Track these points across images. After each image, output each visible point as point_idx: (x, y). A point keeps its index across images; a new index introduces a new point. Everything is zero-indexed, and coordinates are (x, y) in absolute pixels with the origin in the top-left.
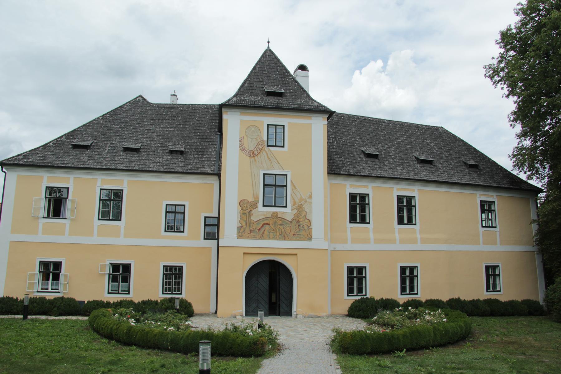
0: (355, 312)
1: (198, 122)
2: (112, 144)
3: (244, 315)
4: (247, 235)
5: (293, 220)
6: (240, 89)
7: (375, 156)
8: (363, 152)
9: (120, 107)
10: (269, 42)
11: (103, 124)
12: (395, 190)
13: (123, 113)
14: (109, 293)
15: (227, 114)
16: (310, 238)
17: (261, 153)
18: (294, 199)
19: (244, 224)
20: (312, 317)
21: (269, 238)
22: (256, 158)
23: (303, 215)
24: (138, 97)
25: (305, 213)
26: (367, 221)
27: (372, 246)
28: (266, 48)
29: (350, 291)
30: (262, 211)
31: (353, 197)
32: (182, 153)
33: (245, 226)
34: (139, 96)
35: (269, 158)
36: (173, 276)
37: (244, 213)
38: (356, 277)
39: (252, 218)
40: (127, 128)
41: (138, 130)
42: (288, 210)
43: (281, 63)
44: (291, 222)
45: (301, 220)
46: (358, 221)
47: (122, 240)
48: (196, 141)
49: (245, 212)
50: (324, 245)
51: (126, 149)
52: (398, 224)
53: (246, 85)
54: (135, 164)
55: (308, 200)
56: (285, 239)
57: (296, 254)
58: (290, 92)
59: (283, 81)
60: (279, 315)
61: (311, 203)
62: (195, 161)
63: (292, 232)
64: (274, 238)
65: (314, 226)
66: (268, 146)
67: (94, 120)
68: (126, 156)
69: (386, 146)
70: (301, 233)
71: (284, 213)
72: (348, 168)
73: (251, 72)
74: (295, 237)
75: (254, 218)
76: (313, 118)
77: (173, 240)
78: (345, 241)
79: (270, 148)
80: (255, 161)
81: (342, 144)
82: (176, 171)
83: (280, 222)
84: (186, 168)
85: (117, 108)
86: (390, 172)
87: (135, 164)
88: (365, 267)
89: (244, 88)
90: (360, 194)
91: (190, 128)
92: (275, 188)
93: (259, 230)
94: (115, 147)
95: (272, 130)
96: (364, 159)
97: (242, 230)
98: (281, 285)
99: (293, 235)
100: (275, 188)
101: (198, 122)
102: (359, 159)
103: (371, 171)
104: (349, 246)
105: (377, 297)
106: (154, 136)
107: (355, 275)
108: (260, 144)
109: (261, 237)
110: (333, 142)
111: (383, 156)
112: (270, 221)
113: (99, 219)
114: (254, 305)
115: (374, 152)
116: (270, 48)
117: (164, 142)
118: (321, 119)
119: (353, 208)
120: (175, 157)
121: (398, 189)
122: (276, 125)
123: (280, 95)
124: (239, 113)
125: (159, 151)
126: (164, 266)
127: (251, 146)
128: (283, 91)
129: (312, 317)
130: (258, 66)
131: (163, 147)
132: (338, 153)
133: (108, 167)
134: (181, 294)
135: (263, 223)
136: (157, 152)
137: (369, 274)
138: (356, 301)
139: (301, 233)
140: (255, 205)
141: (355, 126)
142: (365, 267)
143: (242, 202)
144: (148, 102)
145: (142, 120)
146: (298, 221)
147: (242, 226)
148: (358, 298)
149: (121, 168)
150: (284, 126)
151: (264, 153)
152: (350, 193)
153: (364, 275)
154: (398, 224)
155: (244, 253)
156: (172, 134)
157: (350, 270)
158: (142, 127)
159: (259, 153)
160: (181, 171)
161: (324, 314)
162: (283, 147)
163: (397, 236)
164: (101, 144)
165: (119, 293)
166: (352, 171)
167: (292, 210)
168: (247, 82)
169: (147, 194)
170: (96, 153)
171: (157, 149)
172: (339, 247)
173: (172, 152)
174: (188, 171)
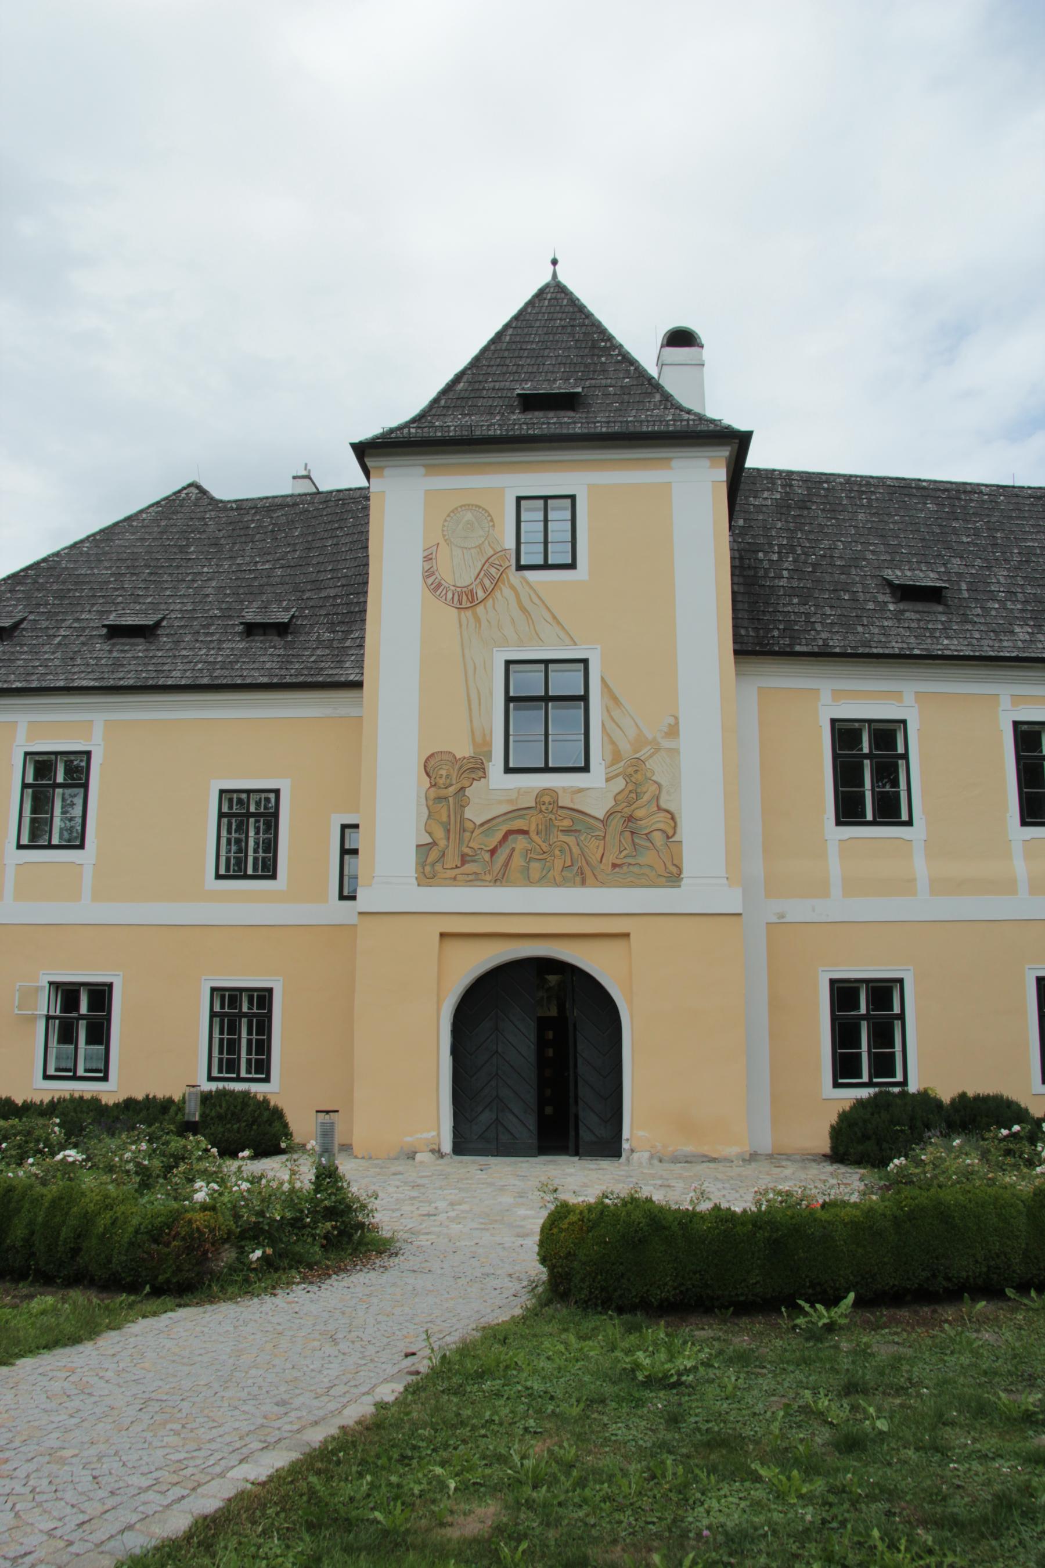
0: (856, 1141)
1: (348, 539)
2: (77, 620)
3: (447, 1146)
4: (452, 873)
5: (610, 814)
6: (435, 401)
7: (932, 595)
8: (889, 583)
9: (129, 519)
10: (554, 262)
11: (66, 568)
12: (1005, 702)
13: (133, 533)
14: (46, 1077)
15: (382, 476)
16: (674, 877)
17: (497, 594)
18: (613, 742)
19: (440, 834)
20: (688, 1160)
21: (529, 881)
22: (480, 609)
23: (646, 797)
24: (184, 488)
25: (654, 788)
26: (905, 817)
27: (923, 906)
28: (547, 278)
29: (845, 1068)
30: (500, 789)
31: (845, 734)
32: (281, 629)
33: (442, 843)
34: (190, 485)
35: (523, 609)
36: (243, 1020)
37: (439, 799)
38: (865, 1018)
39: (468, 813)
40: (133, 574)
41: (165, 577)
42: (596, 778)
43: (589, 315)
44: (605, 822)
45: (640, 813)
46: (869, 817)
47: (86, 910)
48: (332, 592)
49: (443, 793)
50: (731, 901)
51: (115, 632)
52: (1024, 823)
53: (461, 386)
54: (129, 672)
55: (665, 743)
56: (583, 883)
57: (627, 935)
58: (606, 395)
59: (586, 365)
60: (576, 1153)
61: (675, 752)
62: (319, 652)
63: (610, 858)
64: (543, 881)
65: (688, 832)
66: (520, 567)
67: (44, 560)
68: (110, 651)
69: (978, 562)
70: (641, 860)
71: (580, 790)
72: (824, 635)
73: (484, 350)
74: (622, 872)
75: (476, 814)
76: (674, 463)
77: (248, 903)
78: (821, 890)
79: (529, 574)
80: (478, 620)
81: (813, 565)
82: (248, 681)
83: (567, 823)
84: (283, 672)
85: (116, 524)
86: (985, 642)
87: (129, 672)
88: (901, 981)
89: (451, 395)
90: (870, 722)
91: (321, 559)
92: (546, 700)
93: (493, 852)
94: (84, 629)
95: (532, 515)
96: (891, 607)
97: (434, 855)
98: (580, 1047)
99: (614, 866)
100: (546, 700)
101: (348, 539)
102: (871, 606)
103: (912, 640)
104: (836, 907)
105: (946, 1095)
106: (210, 590)
107: (863, 1010)
108: (492, 565)
109: (500, 879)
110: (780, 559)
111: (966, 595)
112: (531, 823)
113: (20, 847)
114: (486, 1117)
115: (928, 579)
116: (562, 279)
117: (235, 606)
118: (706, 463)
119: (846, 773)
120: (257, 643)
121: (1016, 700)
122: (546, 498)
123: (568, 402)
124: (422, 470)
125: (212, 629)
126: (213, 990)
127: (460, 570)
128: (579, 390)
129: (688, 1160)
130: (510, 331)
131: (230, 617)
132: (792, 592)
133: (44, 684)
134: (267, 1080)
135: (505, 828)
136: (207, 634)
137: (915, 1007)
138: (860, 1103)
139: (641, 860)
140: (476, 768)
141: (870, 506)
142: (901, 981)
143: (432, 762)
144: (212, 499)
145: (182, 549)
146: (630, 818)
147: (434, 843)
148: (864, 1093)
149: (85, 683)
150: (573, 498)
151: (507, 591)
152: (833, 721)
153: (897, 1010)
154: (1024, 823)
155: (443, 935)
156: (265, 580)
157: (843, 993)
158: (178, 567)
159: (489, 594)
160: (265, 680)
161: (732, 1150)
162: (572, 566)
163: (1020, 867)
164: (44, 624)
165: (75, 1078)
166: (836, 644)
167: (608, 780)
168: (465, 379)
169: (163, 760)
170: (25, 649)
171: (209, 625)
172: (798, 910)
173: (251, 629)
174: (288, 680)
